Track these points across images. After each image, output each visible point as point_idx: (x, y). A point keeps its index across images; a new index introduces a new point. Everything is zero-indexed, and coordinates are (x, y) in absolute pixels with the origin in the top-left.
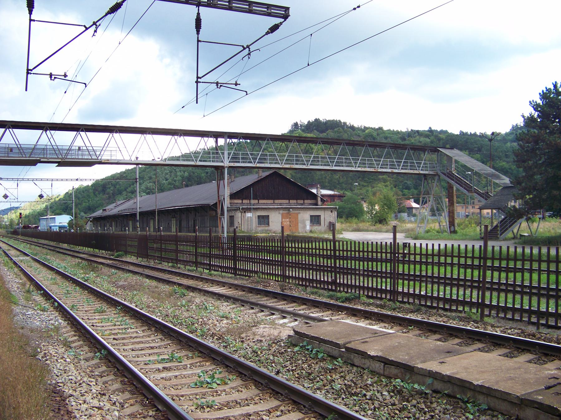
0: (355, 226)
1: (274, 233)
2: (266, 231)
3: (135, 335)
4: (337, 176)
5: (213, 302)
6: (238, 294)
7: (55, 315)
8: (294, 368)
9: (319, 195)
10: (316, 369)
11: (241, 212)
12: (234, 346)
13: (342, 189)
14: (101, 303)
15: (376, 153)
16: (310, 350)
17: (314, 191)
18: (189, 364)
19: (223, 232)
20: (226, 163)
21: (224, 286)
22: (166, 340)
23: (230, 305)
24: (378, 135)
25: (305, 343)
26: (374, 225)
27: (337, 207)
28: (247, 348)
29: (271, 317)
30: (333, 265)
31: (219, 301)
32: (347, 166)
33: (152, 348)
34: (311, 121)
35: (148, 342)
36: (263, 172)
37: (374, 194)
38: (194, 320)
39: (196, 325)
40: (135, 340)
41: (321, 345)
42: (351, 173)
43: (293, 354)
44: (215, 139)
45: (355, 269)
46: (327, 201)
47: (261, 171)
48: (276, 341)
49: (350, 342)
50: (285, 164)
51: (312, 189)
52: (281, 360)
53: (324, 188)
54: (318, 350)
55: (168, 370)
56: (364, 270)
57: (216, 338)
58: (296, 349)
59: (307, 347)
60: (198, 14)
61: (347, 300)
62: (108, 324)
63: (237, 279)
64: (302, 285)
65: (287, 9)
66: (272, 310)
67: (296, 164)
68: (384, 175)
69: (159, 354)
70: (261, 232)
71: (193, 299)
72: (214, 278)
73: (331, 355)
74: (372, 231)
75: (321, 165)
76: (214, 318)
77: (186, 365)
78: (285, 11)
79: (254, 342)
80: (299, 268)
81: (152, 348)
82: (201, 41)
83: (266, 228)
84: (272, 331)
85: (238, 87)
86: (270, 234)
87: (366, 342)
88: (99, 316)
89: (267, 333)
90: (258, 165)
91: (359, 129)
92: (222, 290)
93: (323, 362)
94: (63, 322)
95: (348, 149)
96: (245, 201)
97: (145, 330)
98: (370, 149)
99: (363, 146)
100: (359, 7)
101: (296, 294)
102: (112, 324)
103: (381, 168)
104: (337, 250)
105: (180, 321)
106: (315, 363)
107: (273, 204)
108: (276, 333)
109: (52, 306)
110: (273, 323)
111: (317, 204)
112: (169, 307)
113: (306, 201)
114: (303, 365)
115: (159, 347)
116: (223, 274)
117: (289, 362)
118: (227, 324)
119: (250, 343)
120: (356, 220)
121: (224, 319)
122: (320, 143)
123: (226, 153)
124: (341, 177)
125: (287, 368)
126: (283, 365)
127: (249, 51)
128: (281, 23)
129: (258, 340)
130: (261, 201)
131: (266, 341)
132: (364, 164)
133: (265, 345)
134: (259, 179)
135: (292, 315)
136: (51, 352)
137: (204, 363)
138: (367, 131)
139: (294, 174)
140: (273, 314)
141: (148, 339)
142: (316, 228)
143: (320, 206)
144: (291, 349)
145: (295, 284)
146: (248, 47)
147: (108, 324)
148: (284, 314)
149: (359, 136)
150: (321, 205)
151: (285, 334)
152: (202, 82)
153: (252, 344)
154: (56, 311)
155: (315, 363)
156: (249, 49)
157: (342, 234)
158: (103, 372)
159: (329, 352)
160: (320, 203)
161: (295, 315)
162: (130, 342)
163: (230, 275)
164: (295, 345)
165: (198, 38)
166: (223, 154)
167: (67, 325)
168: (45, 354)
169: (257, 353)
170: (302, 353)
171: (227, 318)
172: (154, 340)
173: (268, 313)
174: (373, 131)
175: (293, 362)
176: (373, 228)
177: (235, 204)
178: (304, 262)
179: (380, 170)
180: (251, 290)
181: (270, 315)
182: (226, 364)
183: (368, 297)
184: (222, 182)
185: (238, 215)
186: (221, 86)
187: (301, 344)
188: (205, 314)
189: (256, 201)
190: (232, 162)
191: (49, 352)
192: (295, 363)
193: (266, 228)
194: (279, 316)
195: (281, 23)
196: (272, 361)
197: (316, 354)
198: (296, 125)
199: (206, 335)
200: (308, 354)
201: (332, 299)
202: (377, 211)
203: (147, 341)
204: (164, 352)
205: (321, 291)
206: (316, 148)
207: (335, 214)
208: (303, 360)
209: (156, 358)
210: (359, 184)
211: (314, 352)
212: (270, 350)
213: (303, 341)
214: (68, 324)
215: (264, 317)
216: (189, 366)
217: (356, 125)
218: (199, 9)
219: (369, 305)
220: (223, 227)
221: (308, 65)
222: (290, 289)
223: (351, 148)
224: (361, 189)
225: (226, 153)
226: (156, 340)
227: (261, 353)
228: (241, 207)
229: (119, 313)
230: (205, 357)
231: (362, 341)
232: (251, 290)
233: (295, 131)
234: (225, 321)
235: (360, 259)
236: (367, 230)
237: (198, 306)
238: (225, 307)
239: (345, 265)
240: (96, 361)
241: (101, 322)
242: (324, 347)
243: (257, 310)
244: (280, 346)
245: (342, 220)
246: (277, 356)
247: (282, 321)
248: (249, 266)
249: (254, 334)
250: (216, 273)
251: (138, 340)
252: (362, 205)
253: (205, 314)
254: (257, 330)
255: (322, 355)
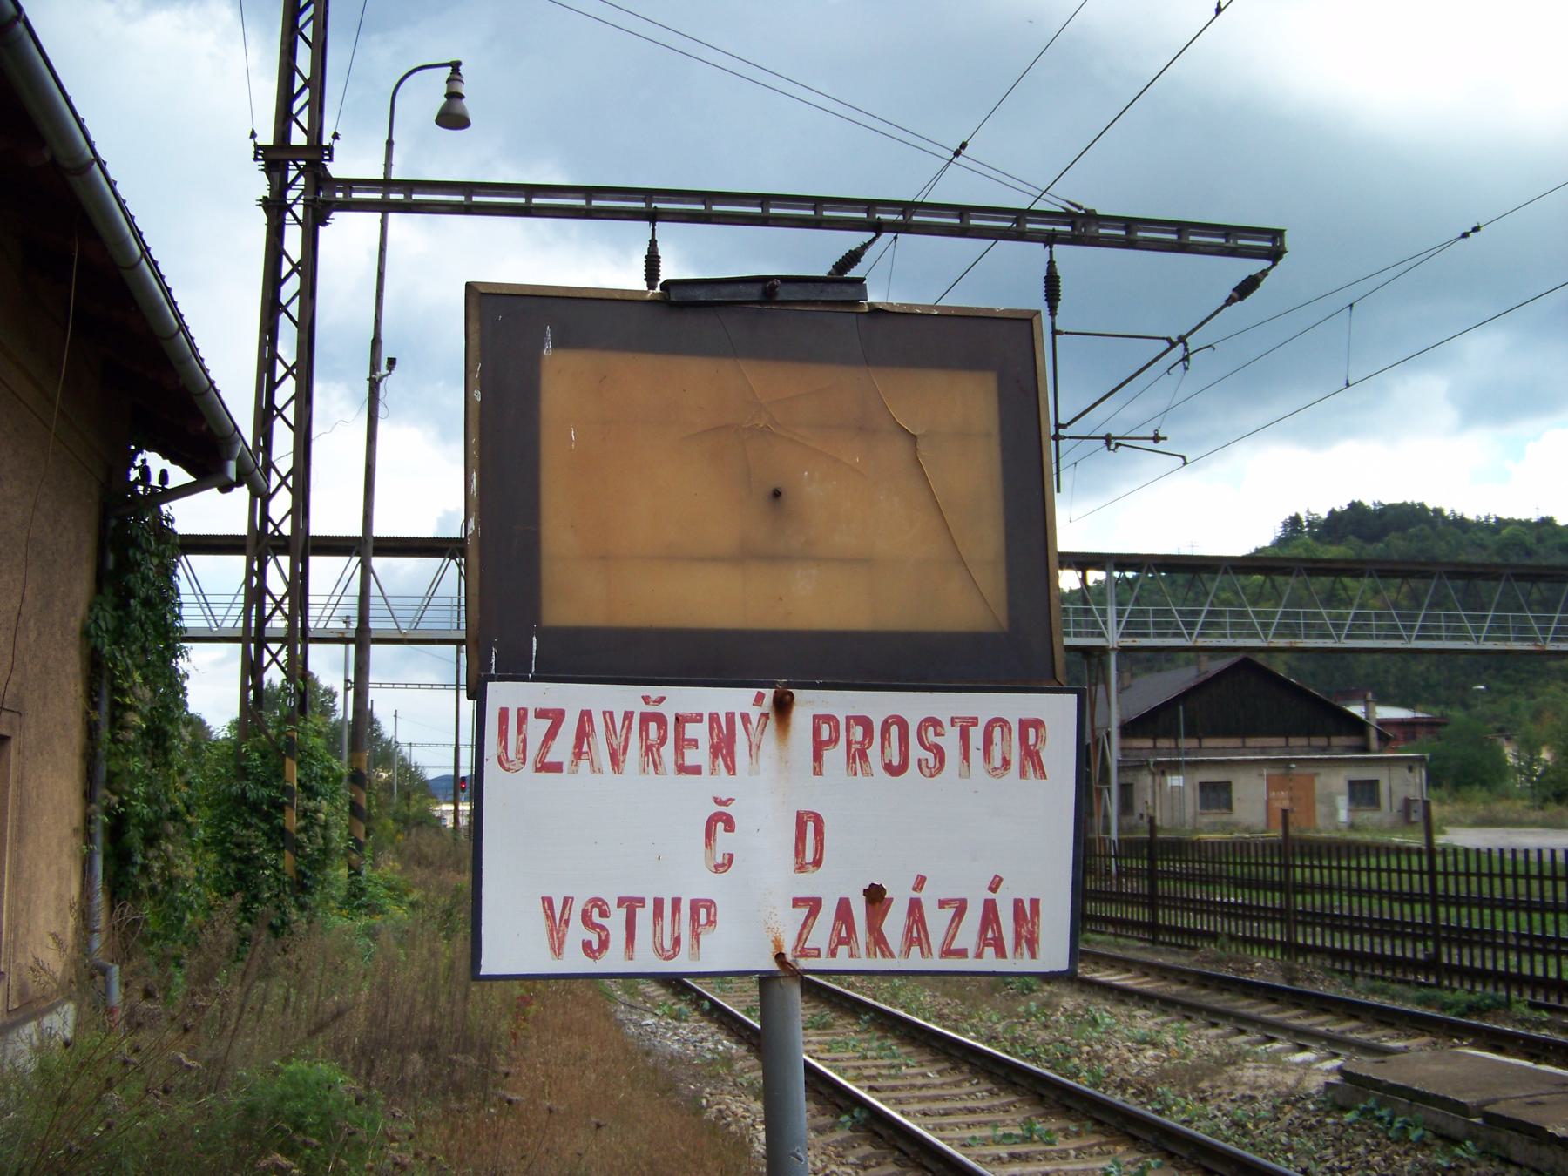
0: (1481, 810)
1: (1247, 830)
2: (1225, 827)
3: (920, 1081)
4: (1419, 667)
5: (1108, 1007)
6: (1173, 989)
7: (709, 1030)
8: (1346, 1164)
9: (1373, 723)
10: (1406, 1169)
11: (1154, 774)
12: (1183, 1111)
13: (1436, 703)
14: (815, 1007)
15: (1535, 595)
16: (1387, 1119)
17: (1357, 710)
18: (1075, 1149)
19: (1107, 829)
20: (1113, 638)
21: (1129, 971)
22: (1002, 1094)
23: (1153, 1017)
24: (1540, 540)
25: (1371, 1103)
26: (1541, 808)
27: (1427, 755)
28: (1215, 1116)
29: (1268, 1046)
30: (1429, 921)
31: (1123, 1007)
32: (1453, 638)
33: (971, 1111)
34: (1338, 509)
35: (953, 1098)
36: (1211, 659)
37: (1537, 716)
38: (1069, 1049)
39: (1076, 1061)
40: (924, 1092)
41: (1414, 1108)
42: (1464, 656)
43: (1341, 1128)
44: (1080, 574)
45: (1493, 933)
46: (1395, 739)
47: (1204, 657)
48: (1294, 1098)
49: (1495, 1101)
50: (1275, 636)
51: (1349, 705)
52: (1310, 1144)
53: (1385, 700)
54: (1409, 1119)
55: (1023, 1161)
56: (1518, 936)
57: (1131, 1090)
58: (1349, 1117)
59: (1377, 1113)
60: (1051, 264)
61: (1472, 1009)
62: (846, 1055)
63: (1159, 953)
64: (1342, 972)
65: (1276, 235)
66: (1270, 1030)
67: (1307, 636)
68: (1564, 658)
69: (995, 1126)
70: (1209, 829)
71: (1055, 1000)
72: (1098, 950)
73: (1444, 1132)
74: (1534, 824)
75: (1378, 637)
76: (1120, 1045)
77: (1066, 1151)
78: (1273, 240)
79: (1233, 1101)
80: (1323, 926)
81: (971, 1111)
82: (1060, 333)
83: (1225, 818)
84: (1279, 1076)
85: (1161, 446)
86: (1236, 835)
87: (1540, 1103)
88: (819, 1035)
89: (1268, 1078)
90: (1202, 642)
91: (1482, 527)
92: (1124, 979)
93: (1422, 1151)
94: (735, 1047)
95: (1452, 588)
96: (1163, 743)
97: (945, 1069)
98: (1519, 588)
99: (1498, 578)
100: (1476, 229)
101: (1331, 993)
102: (857, 1055)
103: (1553, 639)
104: (1440, 873)
105: (1031, 1051)
106: (1401, 1152)
107: (1242, 751)
108: (1290, 1079)
109: (694, 1010)
110: (1274, 1059)
111: (1365, 749)
112: (994, 1018)
113: (1336, 741)
114: (1369, 1158)
115: (990, 1110)
116: (1121, 941)
117: (1330, 1151)
118: (1157, 1058)
119: (1223, 1104)
120: (1484, 794)
121: (1147, 1046)
122: (1371, 576)
123: (1111, 611)
124: (1433, 669)
125: (1328, 1164)
126: (1316, 1156)
127: (1186, 350)
128: (1264, 273)
129: (1243, 1097)
130: (1208, 743)
131: (1264, 1098)
132: (1504, 629)
133: (1264, 1109)
134: (1202, 679)
135: (1324, 1043)
136: (733, 1107)
137: (1111, 1148)
138: (1505, 532)
139: (1294, 663)
140: (1272, 1040)
141: (956, 1091)
142: (1367, 816)
143: (1375, 752)
144: (1334, 1117)
145: (1322, 968)
146: (1182, 339)
147: (846, 1055)
148: (1302, 1039)
149: (1482, 547)
150: (1380, 751)
151: (1315, 1083)
152: (1070, 438)
153: (1227, 1106)
154: (711, 1021)
155: (1401, 1152)
156: (1186, 344)
157: (1443, 833)
158: (867, 1157)
159: (1437, 1126)
160: (1374, 743)
161: (1334, 1043)
162: (914, 1098)
163: (1141, 944)
164: (1345, 1109)
165: (1053, 324)
166: (1103, 613)
167: (746, 1053)
168: (720, 1111)
169: (1244, 1126)
170: (1365, 1127)
171: (1155, 1045)
172: (973, 1093)
173: (1258, 1037)
174: (1524, 529)
175: (1343, 1148)
176: (1537, 815)
177: (1135, 753)
178: (1336, 912)
179: (1551, 646)
180: (1204, 981)
181: (1263, 1043)
182: (1166, 1150)
183: (1534, 1006)
184: (1101, 688)
185: (1145, 780)
186: (1118, 445)
187: (1362, 1106)
188: (1095, 1035)
189: (1194, 743)
190: (1130, 635)
191: (728, 1108)
192: (1348, 1152)
193: (1225, 818)
194: (1288, 1045)
195: (1264, 273)
196: (1285, 1148)
197: (1404, 1129)
198: (1295, 521)
199: (1104, 1085)
200: (1381, 1130)
201: (1429, 1007)
202: (1546, 766)
203: (955, 1096)
204: (1003, 1121)
205: (1397, 987)
206: (1356, 587)
207: (1420, 776)
208: (1367, 1144)
209: (987, 1132)
210: (1488, 688)
211: (1397, 1125)
212: (1278, 1119)
213: (1367, 1097)
214: (748, 1051)
215: (1247, 1047)
216: (1072, 1153)
217: (1471, 516)
218: (1051, 252)
219: (1540, 1025)
220: (1106, 817)
221: (1348, 385)
222: (1308, 978)
223: (1460, 583)
224: (1494, 702)
225: (1111, 611)
226: (979, 1094)
227: (1256, 1126)
228: (1152, 760)
229: (866, 1031)
230: (1112, 1134)
231: (1529, 1100)
232: (1204, 981)
233: (1294, 538)
234: (1150, 1053)
235: (1505, 905)
236: (1518, 823)
237: (1070, 1016)
238: (1145, 1021)
239: (1549, 894)
240: (839, 1135)
241: (829, 1051)
242: (1423, 1112)
243: (1228, 1029)
244: (1306, 1110)
245: (1443, 793)
246: (1298, 1135)
247: (1300, 1057)
248: (1187, 920)
249: (1233, 1082)
250: (1098, 938)
251: (932, 1092)
252: (1500, 750)
253: (1095, 1035)
254: (1240, 1073)
255: (1419, 1132)
